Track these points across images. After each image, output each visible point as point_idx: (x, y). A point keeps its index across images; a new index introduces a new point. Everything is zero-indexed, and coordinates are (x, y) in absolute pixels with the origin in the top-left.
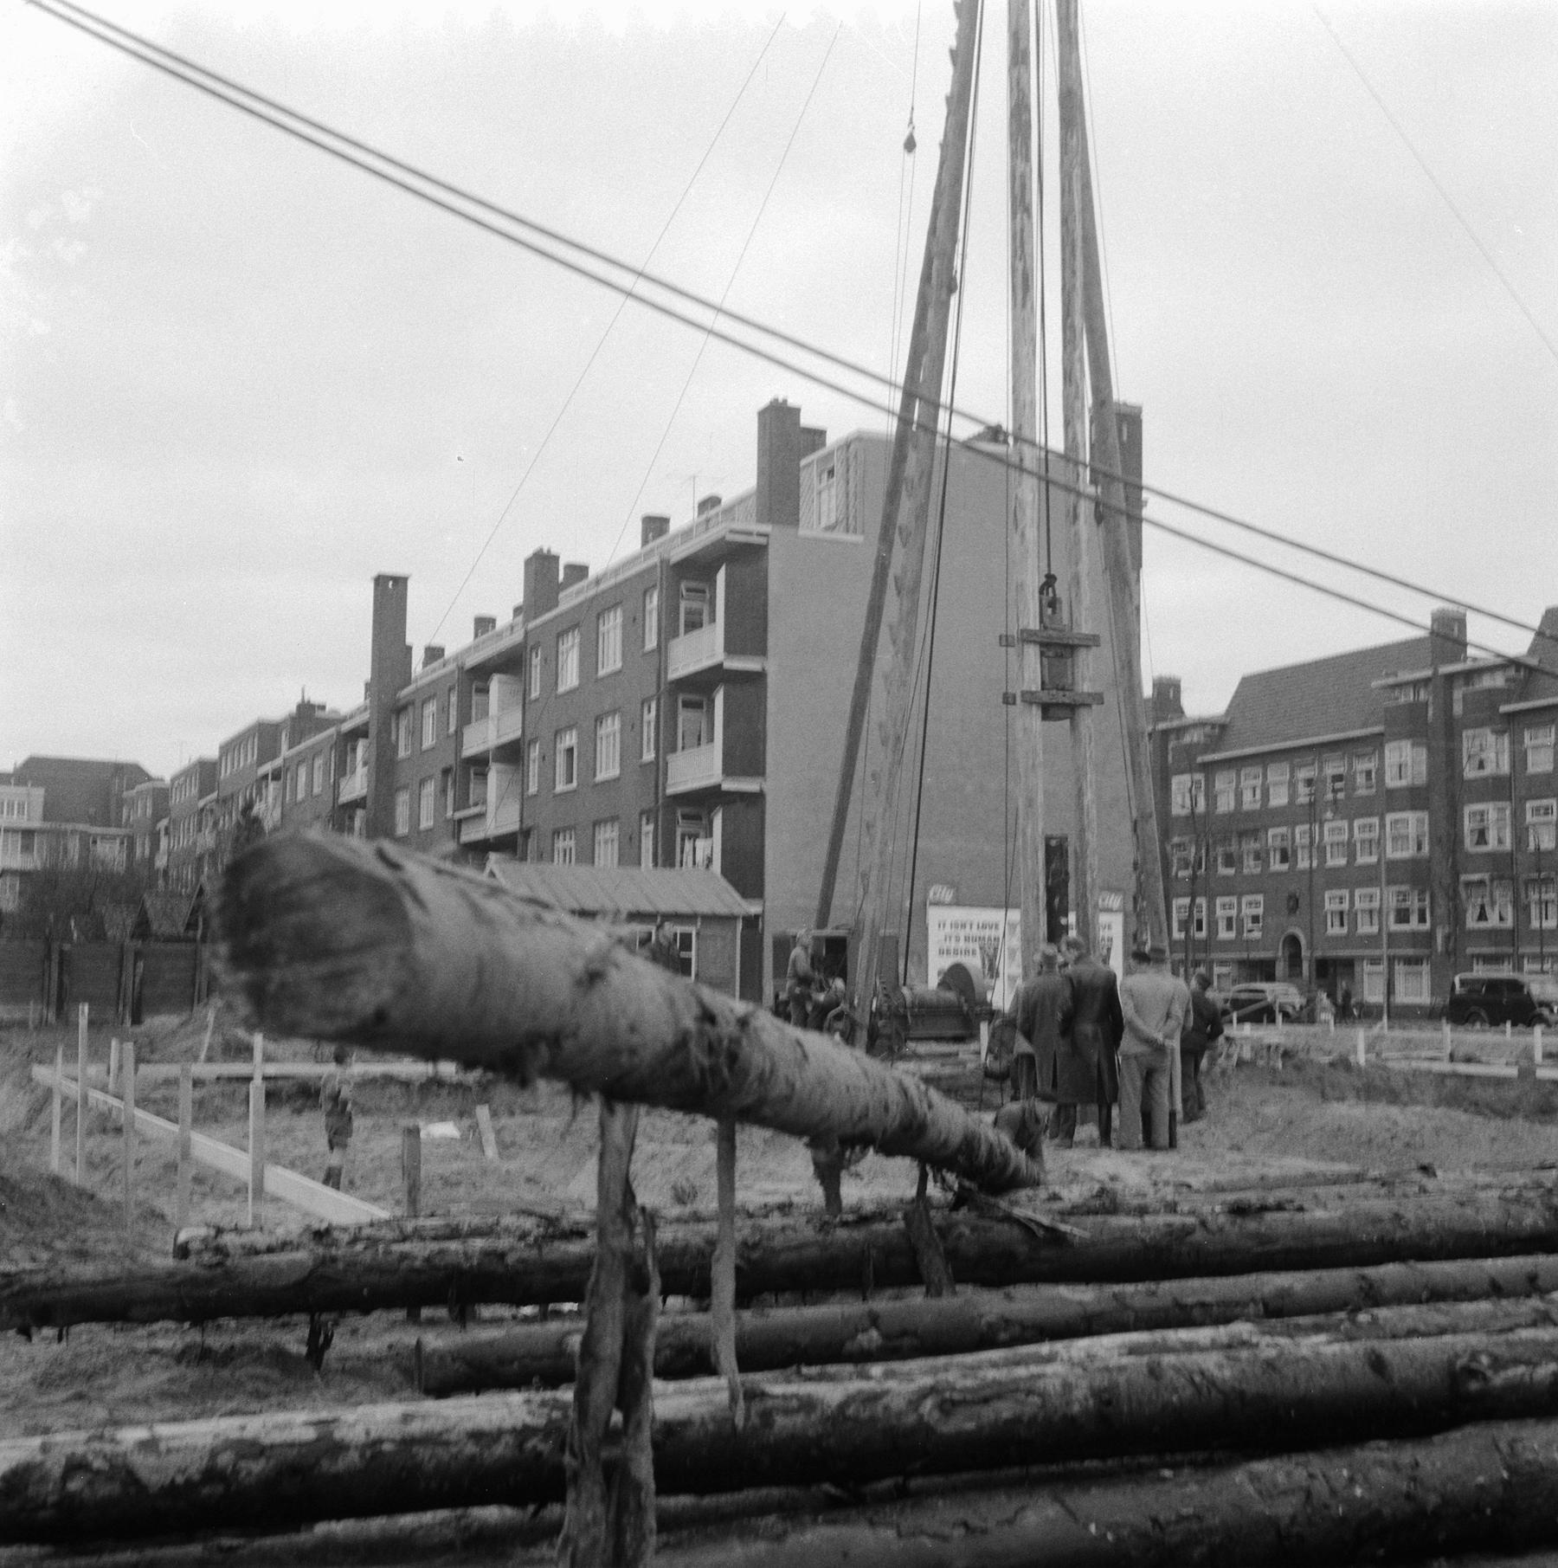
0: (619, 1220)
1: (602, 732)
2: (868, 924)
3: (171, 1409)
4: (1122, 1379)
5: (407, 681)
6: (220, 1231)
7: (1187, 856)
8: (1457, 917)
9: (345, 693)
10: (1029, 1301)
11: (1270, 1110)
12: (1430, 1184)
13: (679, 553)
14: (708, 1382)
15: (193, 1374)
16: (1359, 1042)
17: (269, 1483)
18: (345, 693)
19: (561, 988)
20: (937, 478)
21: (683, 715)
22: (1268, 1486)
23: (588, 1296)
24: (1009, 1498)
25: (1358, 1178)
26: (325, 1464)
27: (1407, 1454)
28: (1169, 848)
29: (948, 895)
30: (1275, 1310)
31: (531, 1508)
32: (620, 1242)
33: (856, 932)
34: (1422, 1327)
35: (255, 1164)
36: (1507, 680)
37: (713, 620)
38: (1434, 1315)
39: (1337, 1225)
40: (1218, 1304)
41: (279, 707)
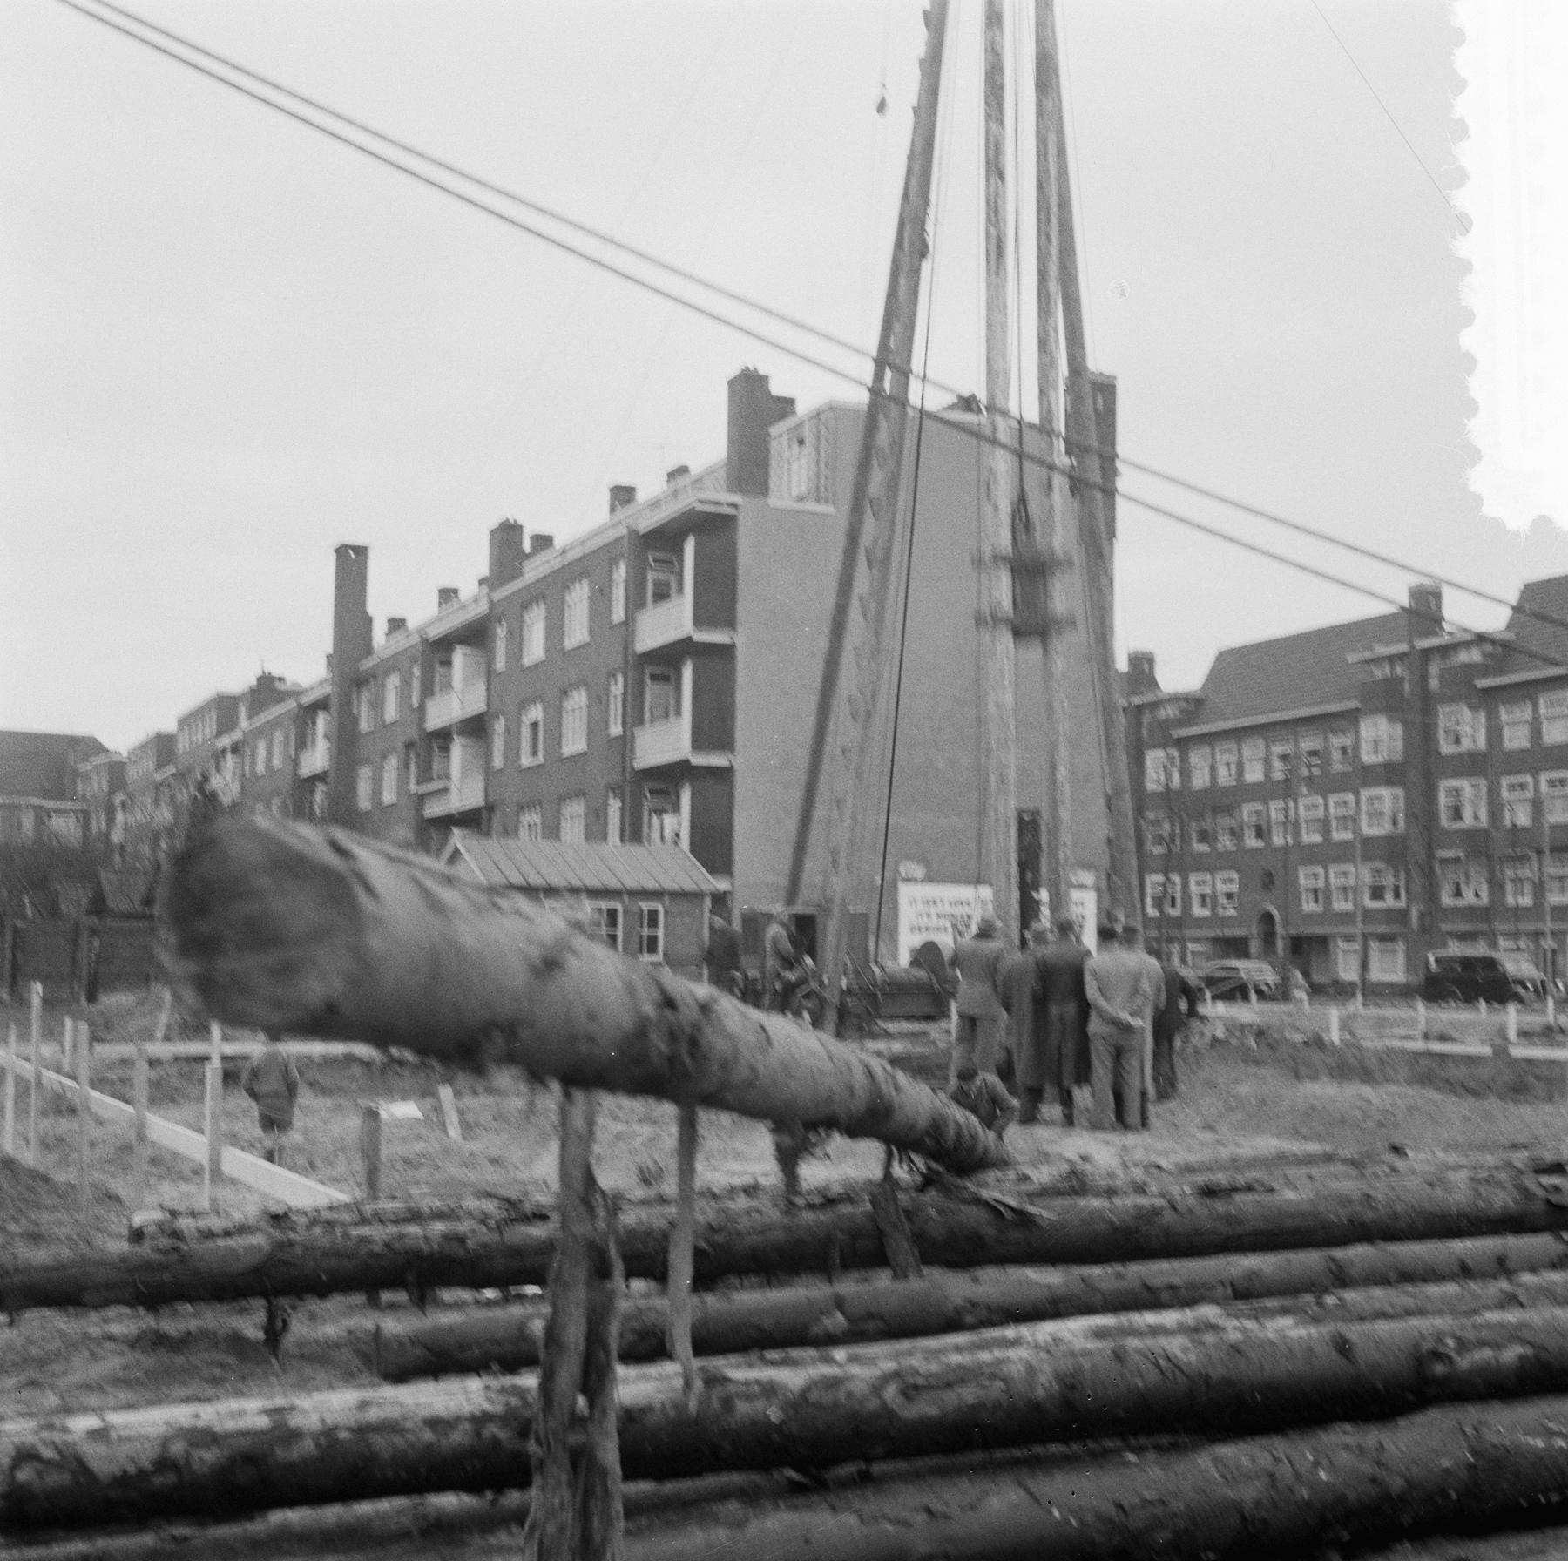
2: (838, 900)
3: (125, 1396)
4: (1087, 1366)
5: (368, 650)
7: (1161, 830)
8: (1432, 895)
11: (1243, 1089)
12: (1399, 1163)
13: (646, 523)
15: (148, 1361)
16: (1332, 1020)
17: (223, 1472)
19: (517, 977)
21: (651, 690)
25: (1329, 1158)
27: (1373, 1436)
30: (1243, 1293)
31: (489, 1495)
34: (1390, 1310)
37: (680, 590)
41: (239, 680)
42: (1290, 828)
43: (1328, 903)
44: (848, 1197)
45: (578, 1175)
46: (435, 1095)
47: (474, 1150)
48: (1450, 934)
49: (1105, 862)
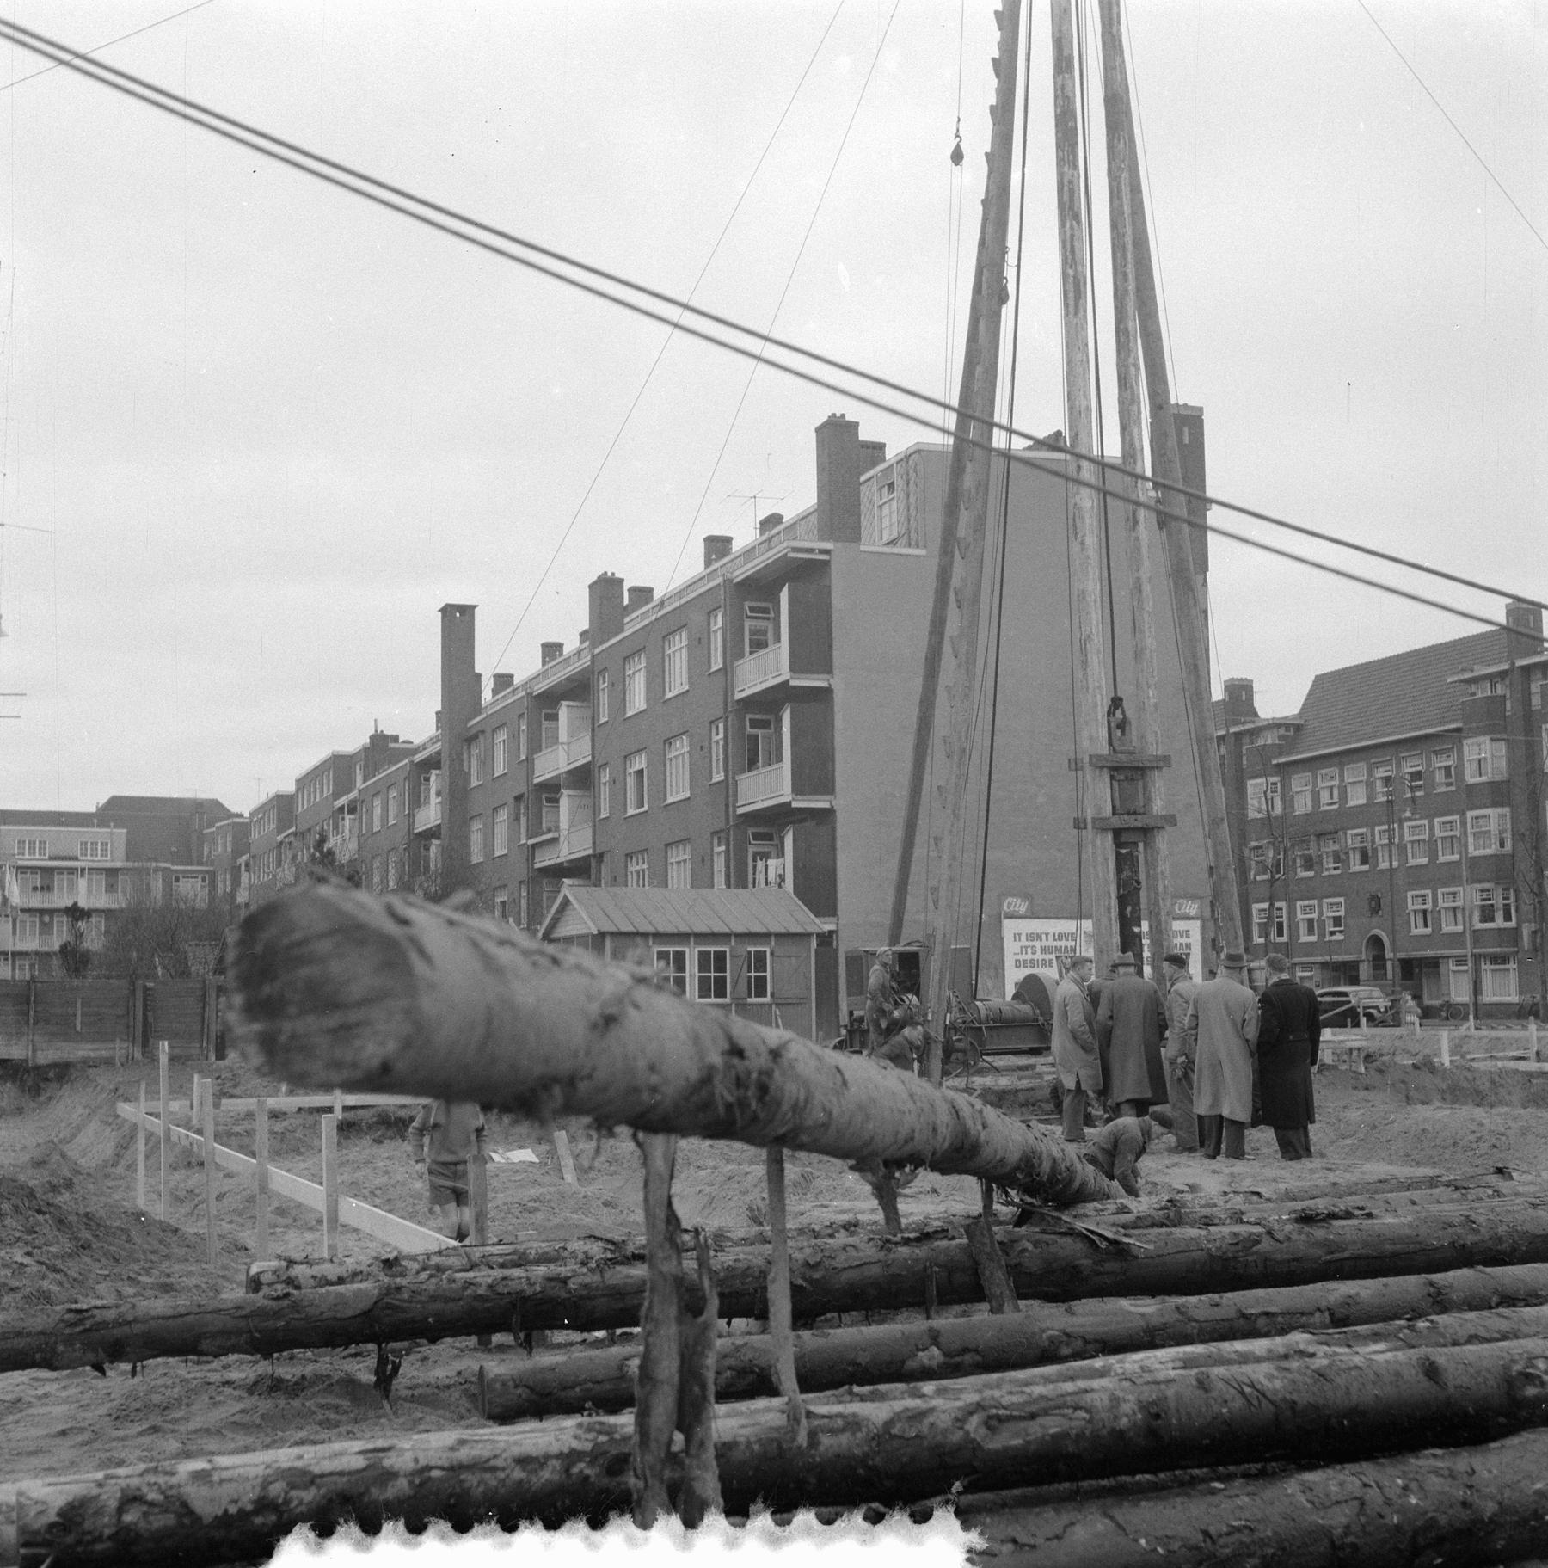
0: (667, 1246)
1: (671, 755)
2: (939, 937)
3: (243, 1440)
4: (1170, 1393)
5: (476, 707)
6: (291, 1262)
7: (1264, 862)
9: (417, 719)
10: (1090, 1314)
11: (1353, 1115)
12: (1504, 1186)
13: (741, 572)
14: (761, 1403)
15: (265, 1405)
16: (1443, 1043)
18: (417, 719)
19: (576, 1033)
22: (1324, 1497)
23: (642, 1321)
24: (1057, 1511)
25: (1433, 1182)
26: (375, 1492)
27: (1463, 1461)
28: (1246, 852)
29: (1022, 908)
30: (1342, 1319)
32: (669, 1267)
33: (929, 949)
34: (1483, 1333)
35: (329, 1196)
37: (778, 639)
38: (1491, 1321)
39: (1408, 1231)
40: (1282, 1314)
41: (353, 741)
42: (1395, 851)
44: (942, 1233)
45: (661, 1214)
46: (551, 1141)
47: (554, 1193)
49: (1207, 891)
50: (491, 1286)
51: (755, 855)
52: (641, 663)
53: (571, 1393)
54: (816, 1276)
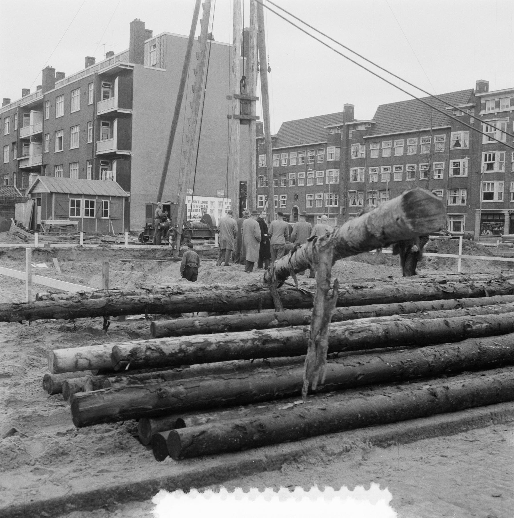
1: (72, 132)
4: (390, 327)
6: (51, 293)
8: (346, 203)
17: (195, 352)
20: (207, 53)
21: (102, 128)
27: (456, 346)
31: (251, 360)
36: (366, 128)
37: (113, 96)
39: (383, 292)
43: (315, 205)
48: (351, 215)
50: (139, 300)
51: (102, 169)
52: (62, 100)
53: (179, 330)
54: (229, 300)
